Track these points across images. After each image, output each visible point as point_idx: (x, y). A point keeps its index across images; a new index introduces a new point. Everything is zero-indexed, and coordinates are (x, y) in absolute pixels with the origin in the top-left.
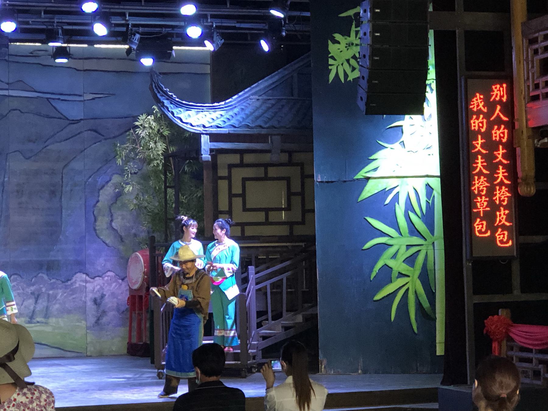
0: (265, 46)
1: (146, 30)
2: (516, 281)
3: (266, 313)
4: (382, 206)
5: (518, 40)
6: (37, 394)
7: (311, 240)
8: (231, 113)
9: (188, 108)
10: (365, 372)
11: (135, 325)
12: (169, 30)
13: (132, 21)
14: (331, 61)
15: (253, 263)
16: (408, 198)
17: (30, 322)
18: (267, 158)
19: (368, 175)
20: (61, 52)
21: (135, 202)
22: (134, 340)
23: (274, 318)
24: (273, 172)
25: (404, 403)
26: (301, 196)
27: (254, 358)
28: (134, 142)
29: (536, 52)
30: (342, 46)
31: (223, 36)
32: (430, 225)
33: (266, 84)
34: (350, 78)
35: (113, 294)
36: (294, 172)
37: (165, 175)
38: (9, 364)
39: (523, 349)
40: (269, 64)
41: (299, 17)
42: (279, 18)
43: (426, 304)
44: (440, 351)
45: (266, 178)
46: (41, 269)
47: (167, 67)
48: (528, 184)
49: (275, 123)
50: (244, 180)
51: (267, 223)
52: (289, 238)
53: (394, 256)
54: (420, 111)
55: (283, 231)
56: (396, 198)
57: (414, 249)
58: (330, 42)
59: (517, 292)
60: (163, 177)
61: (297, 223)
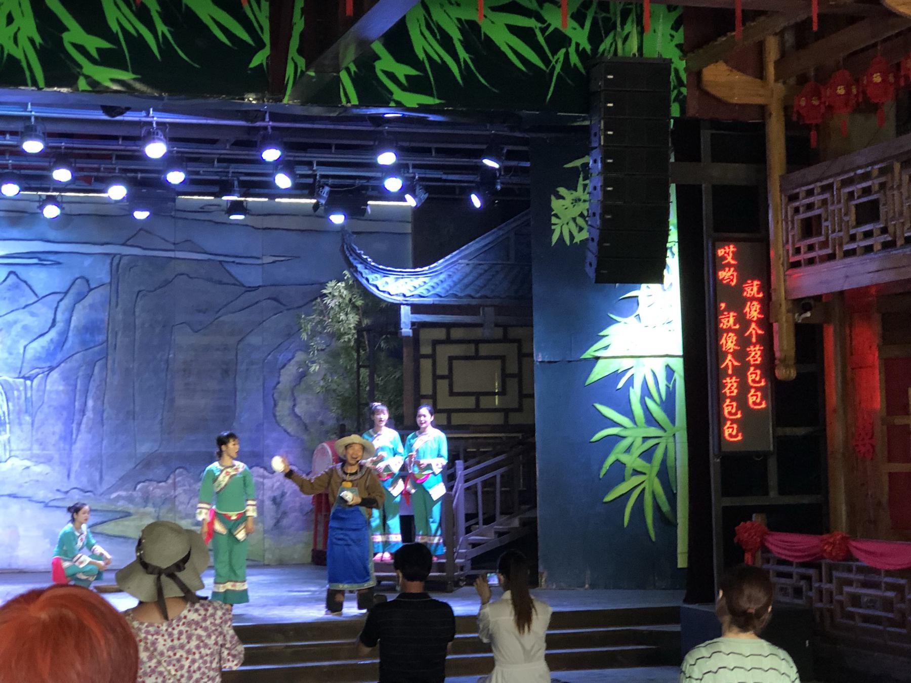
0: (476, 201)
1: (337, 181)
2: (773, 480)
3: (476, 515)
4: (613, 390)
5: (775, 197)
6: (211, 610)
7: (530, 430)
8: (436, 280)
9: (386, 273)
10: (592, 586)
11: (321, 529)
12: (363, 182)
14: (554, 220)
15: (462, 456)
16: (645, 384)
18: (478, 333)
20: (237, 208)
21: (322, 383)
24: (484, 350)
26: (518, 378)
27: (462, 569)
28: (321, 313)
29: (797, 210)
30: (567, 202)
31: (427, 189)
33: (478, 246)
34: (577, 240)
36: (510, 350)
37: (358, 352)
39: (781, 562)
43: (665, 508)
44: (682, 562)
45: (477, 357)
48: (787, 366)
50: (451, 359)
51: (477, 409)
52: (503, 427)
53: (628, 450)
54: (659, 279)
55: (496, 419)
58: (553, 198)
59: (773, 494)
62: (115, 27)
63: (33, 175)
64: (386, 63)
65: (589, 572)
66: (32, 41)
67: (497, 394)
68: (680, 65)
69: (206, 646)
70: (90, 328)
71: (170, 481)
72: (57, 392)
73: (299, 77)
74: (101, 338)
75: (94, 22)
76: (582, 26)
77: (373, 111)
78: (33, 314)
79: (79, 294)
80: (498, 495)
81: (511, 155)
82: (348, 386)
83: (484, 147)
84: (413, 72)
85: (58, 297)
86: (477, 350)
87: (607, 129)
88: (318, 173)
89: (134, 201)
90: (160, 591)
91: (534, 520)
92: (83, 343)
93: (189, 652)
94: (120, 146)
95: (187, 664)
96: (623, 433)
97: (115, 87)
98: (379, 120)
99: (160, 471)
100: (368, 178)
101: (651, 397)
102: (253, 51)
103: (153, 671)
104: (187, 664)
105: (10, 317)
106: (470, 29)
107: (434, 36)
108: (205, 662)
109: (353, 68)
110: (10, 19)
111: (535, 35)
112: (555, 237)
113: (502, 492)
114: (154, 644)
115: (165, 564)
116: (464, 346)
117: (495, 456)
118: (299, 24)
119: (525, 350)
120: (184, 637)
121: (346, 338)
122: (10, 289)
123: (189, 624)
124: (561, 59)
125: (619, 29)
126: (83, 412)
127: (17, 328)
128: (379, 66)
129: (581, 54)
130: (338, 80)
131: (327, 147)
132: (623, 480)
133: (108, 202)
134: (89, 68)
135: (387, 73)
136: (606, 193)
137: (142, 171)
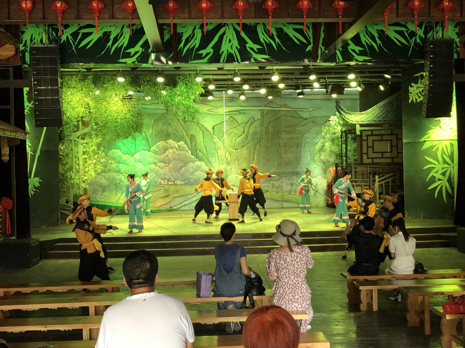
0: (382, 88)
1: (334, 83)
4: (431, 152)
7: (401, 164)
8: (368, 116)
9: (351, 114)
12: (342, 83)
13: (328, 80)
14: (410, 94)
15: (377, 173)
16: (443, 149)
18: (383, 132)
19: (425, 140)
24: (384, 138)
25: (441, 233)
26: (397, 147)
28: (329, 126)
30: (415, 88)
31: (365, 84)
32: (452, 160)
33: (382, 104)
34: (418, 101)
35: (321, 184)
36: (394, 138)
37: (341, 139)
38: (294, 237)
40: (383, 96)
42: (388, 79)
43: (450, 191)
45: (382, 140)
49: (386, 119)
50: (373, 141)
51: (382, 157)
52: (392, 164)
53: (437, 172)
55: (389, 161)
56: (437, 149)
57: (446, 169)
58: (409, 87)
60: (340, 140)
61: (395, 158)
62: (262, 41)
63: (237, 87)
64: (352, 46)
65: (422, 213)
66: (237, 48)
68: (457, 40)
69: (302, 260)
70: (255, 133)
71: (281, 181)
72: (245, 153)
74: (258, 136)
75: (256, 40)
76: (421, 29)
77: (347, 63)
78: (237, 130)
81: (395, 72)
82: (338, 150)
83: (385, 70)
84: (361, 49)
85: (245, 124)
87: (430, 64)
89: (269, 94)
90: (289, 243)
91: (403, 195)
92: (253, 138)
93: (297, 262)
94: (264, 77)
95: (296, 266)
96: (435, 166)
97: (263, 61)
98: (349, 65)
101: (445, 154)
102: (307, 46)
103: (286, 268)
104: (296, 266)
105: (231, 131)
106: (381, 33)
108: (302, 266)
109: (341, 49)
110: (230, 41)
112: (410, 101)
114: (286, 259)
115: (289, 234)
118: (322, 35)
120: (295, 257)
121: (337, 134)
122: (230, 122)
123: (297, 253)
124: (414, 41)
126: (253, 159)
127: (233, 134)
128: (349, 48)
129: (421, 39)
130: (336, 53)
132: (435, 182)
133: (259, 93)
134: (254, 55)
136: (430, 87)
137: (270, 83)
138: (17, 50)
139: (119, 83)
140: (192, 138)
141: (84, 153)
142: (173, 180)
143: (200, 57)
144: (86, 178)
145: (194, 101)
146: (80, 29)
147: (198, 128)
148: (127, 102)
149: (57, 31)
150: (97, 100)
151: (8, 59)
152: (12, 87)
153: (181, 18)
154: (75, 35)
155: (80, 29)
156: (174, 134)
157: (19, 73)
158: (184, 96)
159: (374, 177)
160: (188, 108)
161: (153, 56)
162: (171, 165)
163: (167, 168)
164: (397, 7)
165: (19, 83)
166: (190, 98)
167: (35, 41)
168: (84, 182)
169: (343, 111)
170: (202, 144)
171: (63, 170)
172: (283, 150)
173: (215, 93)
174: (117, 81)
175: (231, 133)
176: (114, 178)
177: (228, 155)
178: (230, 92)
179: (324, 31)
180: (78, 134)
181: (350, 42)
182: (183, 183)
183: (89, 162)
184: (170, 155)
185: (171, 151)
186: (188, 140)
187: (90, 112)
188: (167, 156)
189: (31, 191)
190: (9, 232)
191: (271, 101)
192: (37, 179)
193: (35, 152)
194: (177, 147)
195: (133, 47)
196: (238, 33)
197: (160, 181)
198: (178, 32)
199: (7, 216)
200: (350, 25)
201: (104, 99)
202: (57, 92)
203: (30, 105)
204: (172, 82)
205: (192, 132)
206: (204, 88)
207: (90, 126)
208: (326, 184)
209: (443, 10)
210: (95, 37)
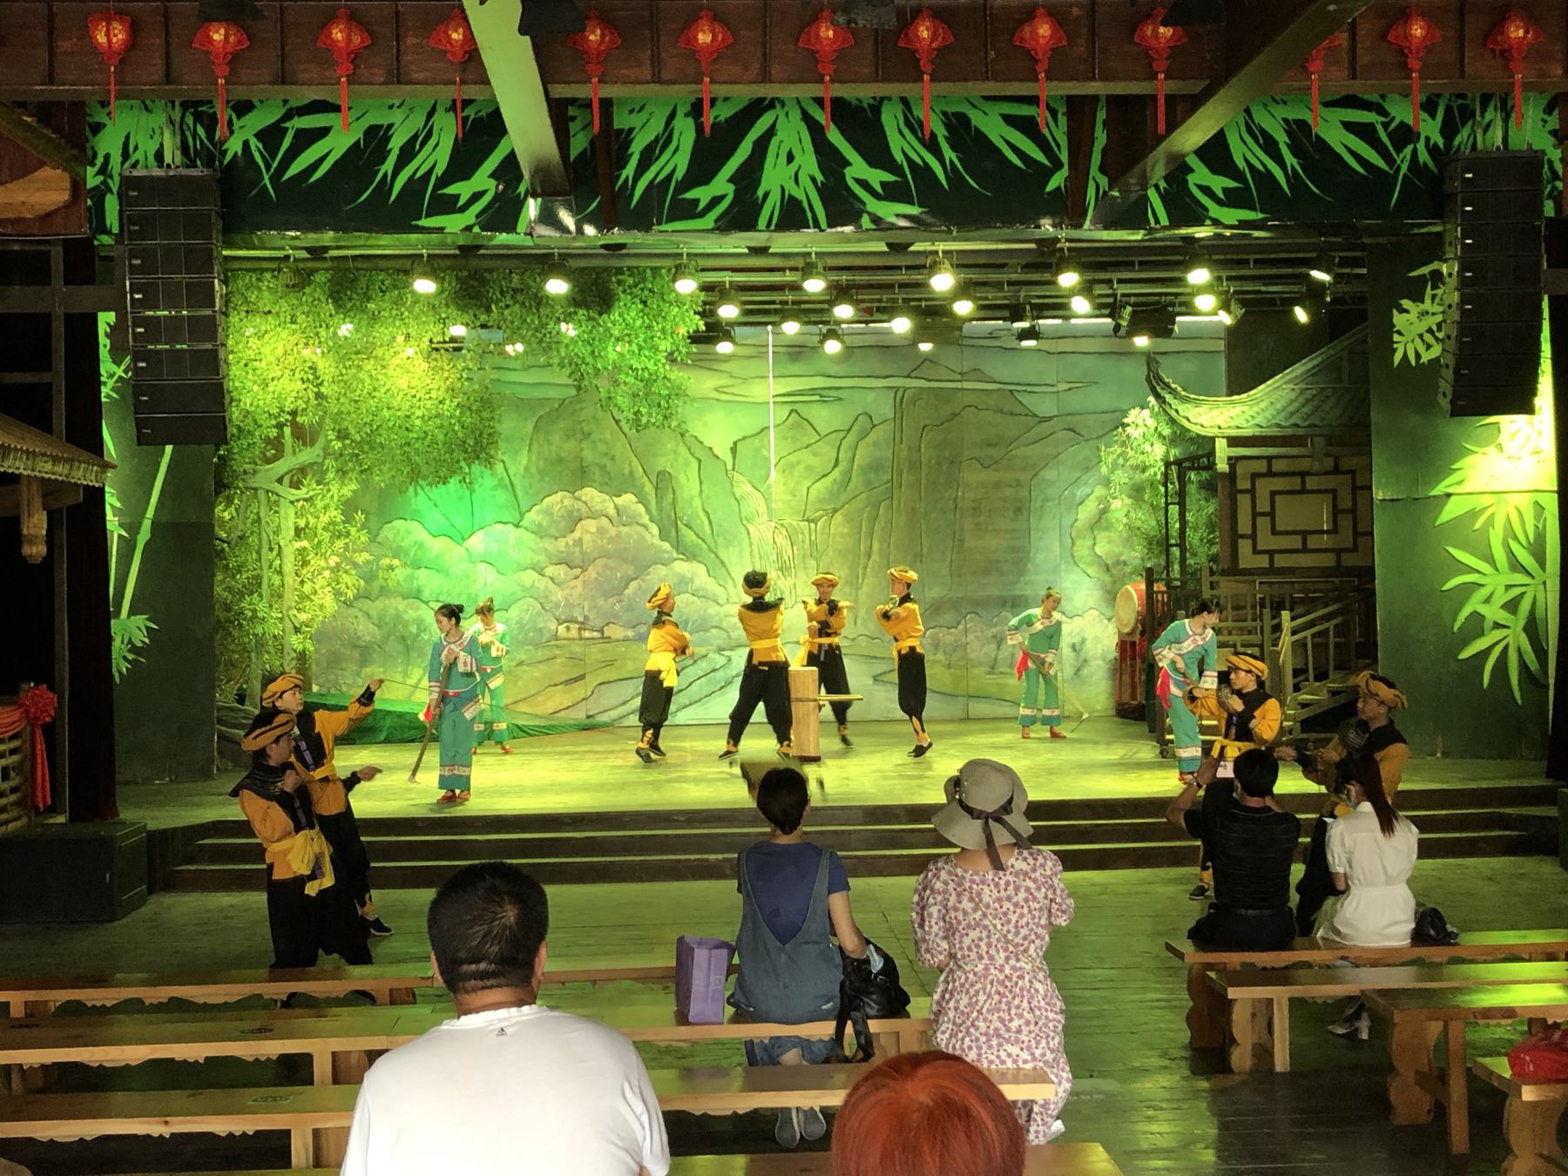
0: (1301, 315)
3: (1305, 671)
4: (1467, 531)
6: (1040, 859)
7: (1369, 573)
8: (1256, 409)
9: (1197, 403)
10: (1445, 755)
11: (1126, 678)
13: (1121, 290)
14: (1396, 337)
17: (990, 673)
18: (1304, 465)
19: (1450, 490)
20: (1031, 333)
21: (1125, 520)
22: (1126, 698)
23: (1317, 679)
26: (1354, 515)
27: (1290, 732)
28: (1123, 444)
30: (1413, 316)
31: (1243, 303)
33: (1305, 368)
34: (1424, 359)
36: (1341, 483)
38: (1006, 818)
40: (1305, 342)
41: (1349, 275)
42: (1322, 284)
43: (1533, 665)
46: (1004, 606)
47: (1166, 344)
50: (1273, 494)
51: (1305, 550)
52: (1338, 570)
53: (1487, 600)
54: (1526, 407)
55: (1328, 560)
56: (1490, 522)
58: (1395, 312)
60: (1162, 489)
63: (814, 312)
64: (1200, 175)
66: (813, 179)
67: (1326, 532)
68: (1555, 155)
69: (1035, 899)
70: (874, 467)
72: (843, 535)
73: (1102, 198)
74: (886, 477)
75: (878, 155)
76: (1433, 117)
77: (1184, 231)
78: (815, 454)
79: (861, 431)
80: (1331, 646)
81: (1344, 262)
83: (1314, 255)
85: (842, 434)
86: (1303, 483)
87: (1465, 236)
88: (1119, 292)
89: (921, 333)
92: (867, 483)
93: (1016, 905)
95: (1014, 918)
97: (903, 223)
98: (1189, 240)
99: (949, 617)
100: (1176, 295)
101: (1516, 538)
102: (1048, 174)
103: (978, 925)
104: (1014, 918)
105: (793, 458)
106: (1299, 132)
107: (1256, 141)
109: (1162, 184)
110: (790, 158)
111: (1376, 131)
113: (1336, 644)
114: (979, 894)
116: (1287, 480)
117: (1326, 606)
118: (1101, 138)
119: (1360, 481)
120: (1011, 888)
121: (1152, 471)
123: (1017, 875)
125: (1478, 118)
127: (800, 469)
128: (1192, 180)
129: (1433, 150)
130: (1146, 198)
131: (1129, 265)
133: (888, 333)
134: (872, 205)
135: (1200, 187)
136: (1463, 312)
138: (77, 185)
139: (417, 298)
140: (663, 482)
141: (298, 532)
142: (598, 623)
143: (689, 211)
144: (303, 617)
145: (671, 358)
146: (288, 116)
147: (683, 450)
148: (443, 360)
149: (210, 123)
150: (347, 354)
151: (47, 217)
152: (59, 312)
153: (626, 81)
154: (271, 136)
155: (288, 116)
156: (602, 467)
157: (83, 263)
158: (633, 342)
159: (1276, 615)
160: (648, 383)
161: (532, 208)
162: (592, 573)
163: (578, 583)
164: (1353, 48)
165: (83, 297)
166: (655, 349)
167: (139, 155)
168: (297, 630)
169: (1173, 392)
170: (697, 503)
171: (229, 589)
172: (968, 524)
173: (739, 332)
174: (413, 293)
175: (793, 466)
176: (398, 618)
177: (782, 541)
178: (791, 328)
179: (1104, 123)
180: (281, 467)
181: (1193, 161)
182: (630, 633)
183: (316, 562)
184: (587, 538)
185: (590, 525)
186: (649, 488)
187: (319, 395)
188: (579, 542)
189: (120, 662)
190: (44, 797)
191: (927, 359)
192: (141, 620)
193: (133, 528)
194: (611, 511)
195: (467, 177)
196: (816, 131)
197: (553, 626)
198: (616, 126)
199: (40, 746)
200: (1194, 103)
201: (366, 351)
202: (208, 329)
203: (120, 372)
204: (595, 293)
205: (663, 463)
206: (702, 314)
207: (320, 443)
208: (1115, 640)
209: (1506, 54)
210: (337, 144)
